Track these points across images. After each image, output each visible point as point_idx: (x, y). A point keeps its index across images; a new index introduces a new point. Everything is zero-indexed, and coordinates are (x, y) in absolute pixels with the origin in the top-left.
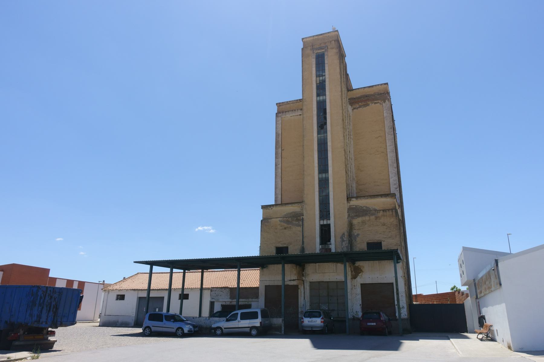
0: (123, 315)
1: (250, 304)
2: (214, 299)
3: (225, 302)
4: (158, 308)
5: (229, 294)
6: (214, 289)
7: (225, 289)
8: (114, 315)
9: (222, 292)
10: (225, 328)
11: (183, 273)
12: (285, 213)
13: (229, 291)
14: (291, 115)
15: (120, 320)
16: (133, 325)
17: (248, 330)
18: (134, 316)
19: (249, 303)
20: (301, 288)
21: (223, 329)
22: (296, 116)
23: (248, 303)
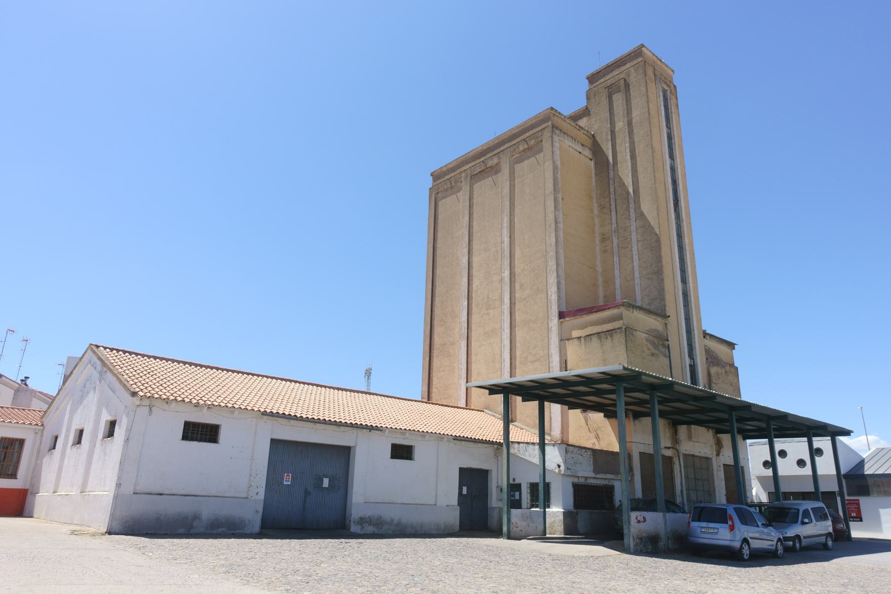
0: (214, 493)
1: (612, 484)
2: (570, 469)
3: (578, 477)
4: (326, 477)
5: (592, 461)
6: (570, 447)
7: (586, 452)
8: (174, 492)
9: (582, 455)
10: (805, 537)
11: (808, 442)
12: (648, 328)
13: (592, 457)
14: (571, 144)
15: (207, 512)
16: (257, 528)
17: (823, 539)
18: (263, 497)
19: (611, 483)
20: (676, 460)
21: (802, 538)
22: (575, 151)
23: (609, 482)
